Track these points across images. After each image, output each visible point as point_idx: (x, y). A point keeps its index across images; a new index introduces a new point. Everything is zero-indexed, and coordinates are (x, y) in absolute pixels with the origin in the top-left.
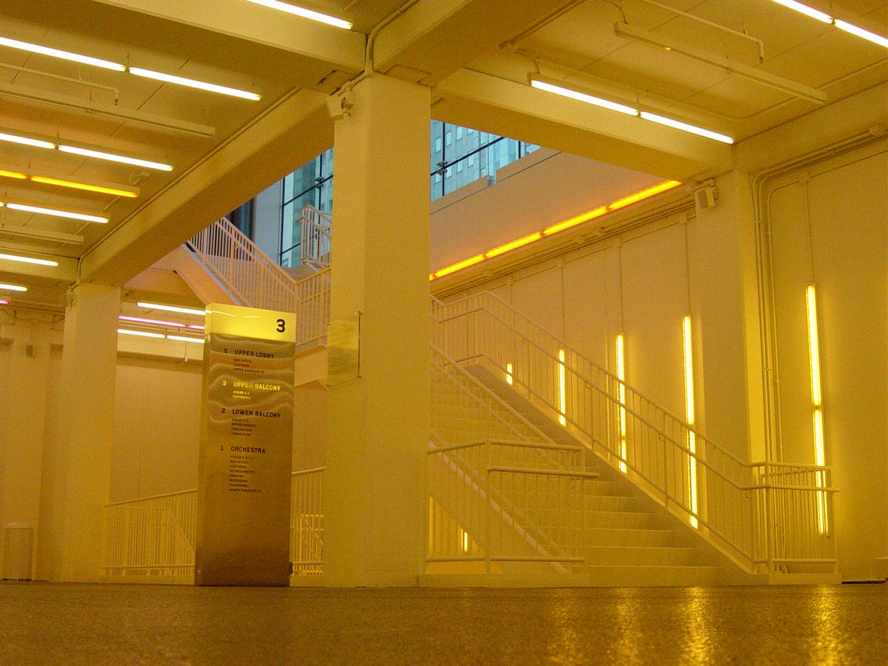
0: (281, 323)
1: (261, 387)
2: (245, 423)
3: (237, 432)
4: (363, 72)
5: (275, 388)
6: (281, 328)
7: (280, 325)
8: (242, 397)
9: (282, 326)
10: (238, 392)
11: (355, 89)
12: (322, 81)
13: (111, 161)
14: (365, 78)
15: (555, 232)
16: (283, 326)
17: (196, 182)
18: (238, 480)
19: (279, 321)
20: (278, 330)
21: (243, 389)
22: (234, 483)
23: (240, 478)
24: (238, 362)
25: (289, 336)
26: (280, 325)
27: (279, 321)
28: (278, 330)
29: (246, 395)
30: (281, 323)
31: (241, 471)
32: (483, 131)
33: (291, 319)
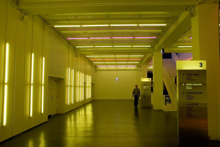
0: (201, 64)
1: (195, 85)
2: (191, 96)
3: (188, 99)
4: (196, 5)
5: (200, 85)
6: (201, 66)
7: (200, 65)
8: (190, 88)
9: (201, 65)
10: (188, 87)
11: (195, 9)
12: (186, 9)
13: (33, 100)
14: (196, 6)
15: (170, 111)
16: (202, 65)
17: (173, 28)
18: (189, 114)
19: (200, 63)
20: (200, 66)
21: (190, 86)
22: (188, 115)
23: (190, 113)
24: (187, 78)
25: (204, 67)
26: (200, 65)
27: (200, 63)
28: (200, 66)
29: (191, 88)
30: (201, 64)
31: (190, 111)
32: (94, 111)
33: (204, 62)
